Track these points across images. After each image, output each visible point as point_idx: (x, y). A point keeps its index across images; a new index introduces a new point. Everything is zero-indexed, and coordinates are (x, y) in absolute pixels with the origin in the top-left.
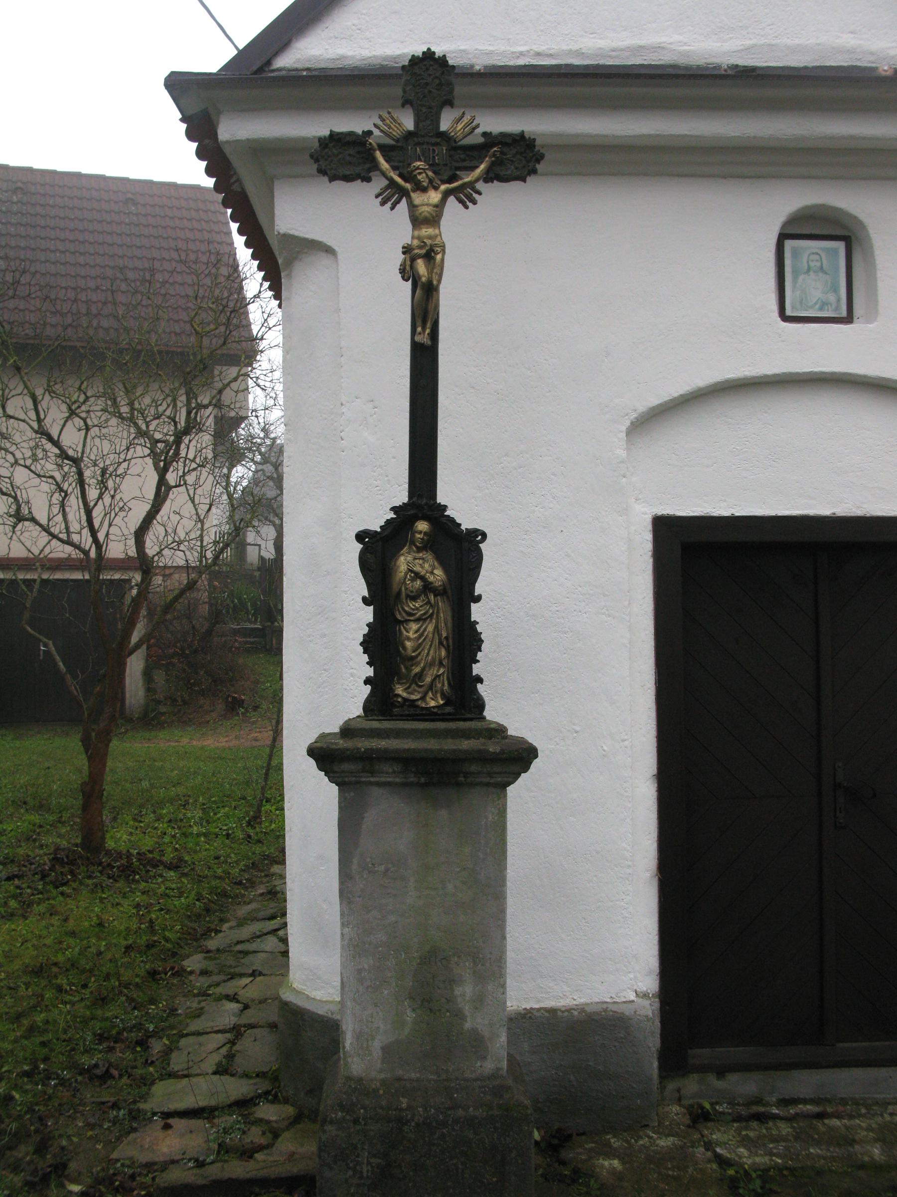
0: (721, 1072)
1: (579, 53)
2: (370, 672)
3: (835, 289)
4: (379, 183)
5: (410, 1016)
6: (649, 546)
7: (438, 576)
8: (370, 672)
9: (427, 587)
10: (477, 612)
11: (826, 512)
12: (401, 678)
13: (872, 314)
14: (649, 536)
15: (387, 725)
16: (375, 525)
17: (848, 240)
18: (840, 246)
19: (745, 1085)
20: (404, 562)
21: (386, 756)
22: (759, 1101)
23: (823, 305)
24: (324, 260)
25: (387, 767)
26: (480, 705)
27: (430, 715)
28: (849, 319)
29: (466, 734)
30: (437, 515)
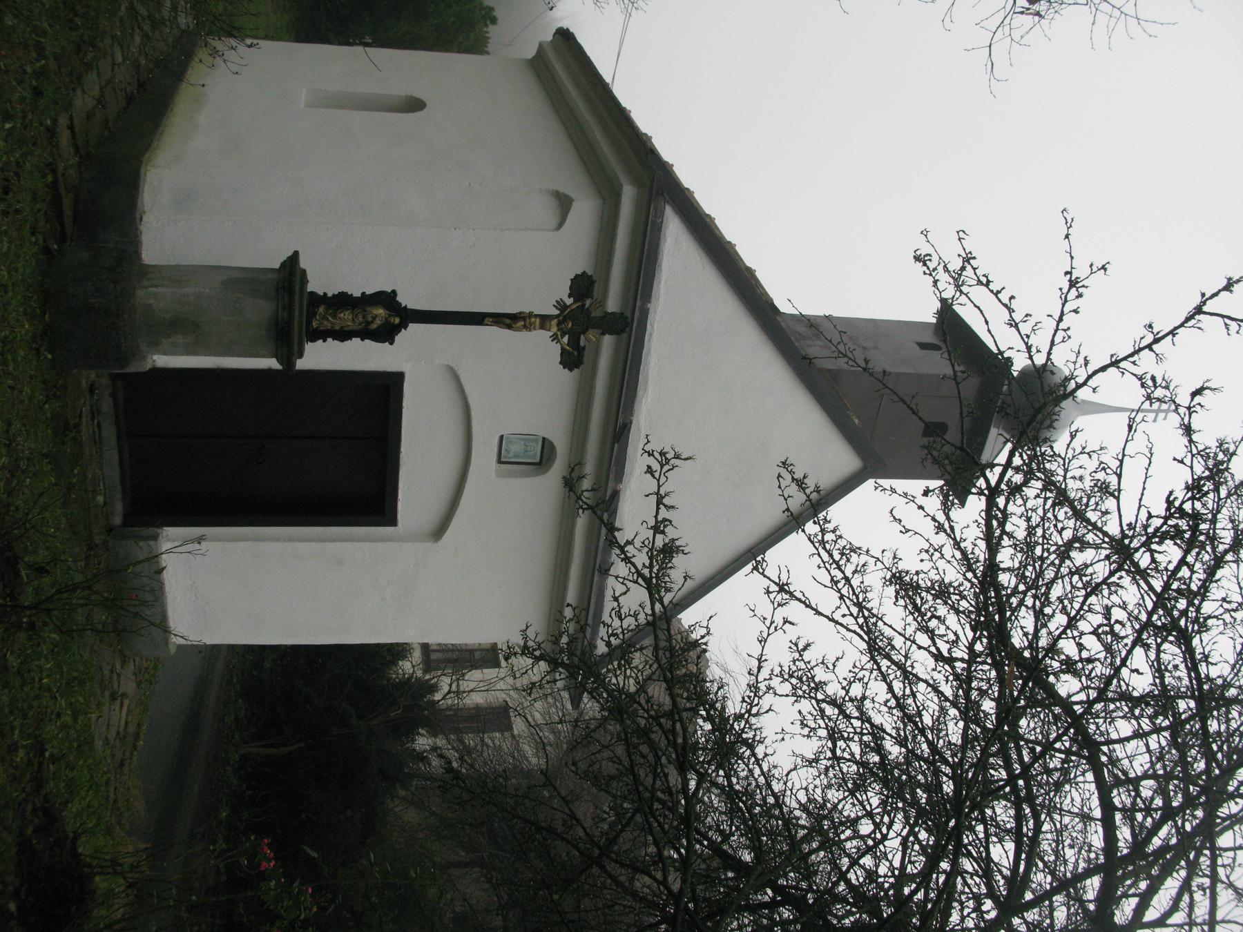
0: (113, 395)
1: (649, 353)
2: (330, 295)
3: (515, 456)
4: (569, 301)
5: (168, 316)
6: (389, 370)
7: (374, 326)
8: (330, 295)
9: (368, 323)
10: (356, 341)
11: (402, 449)
12: (326, 310)
13: (500, 475)
14: (394, 370)
15: (305, 303)
16: (399, 299)
17: (540, 464)
18: (537, 460)
19: (107, 406)
20: (380, 311)
21: (290, 308)
22: (99, 412)
23: (508, 451)
24: (554, 222)
25: (285, 315)
26: (313, 341)
27: (309, 322)
28: (500, 461)
29: (300, 331)
30: (403, 325)
